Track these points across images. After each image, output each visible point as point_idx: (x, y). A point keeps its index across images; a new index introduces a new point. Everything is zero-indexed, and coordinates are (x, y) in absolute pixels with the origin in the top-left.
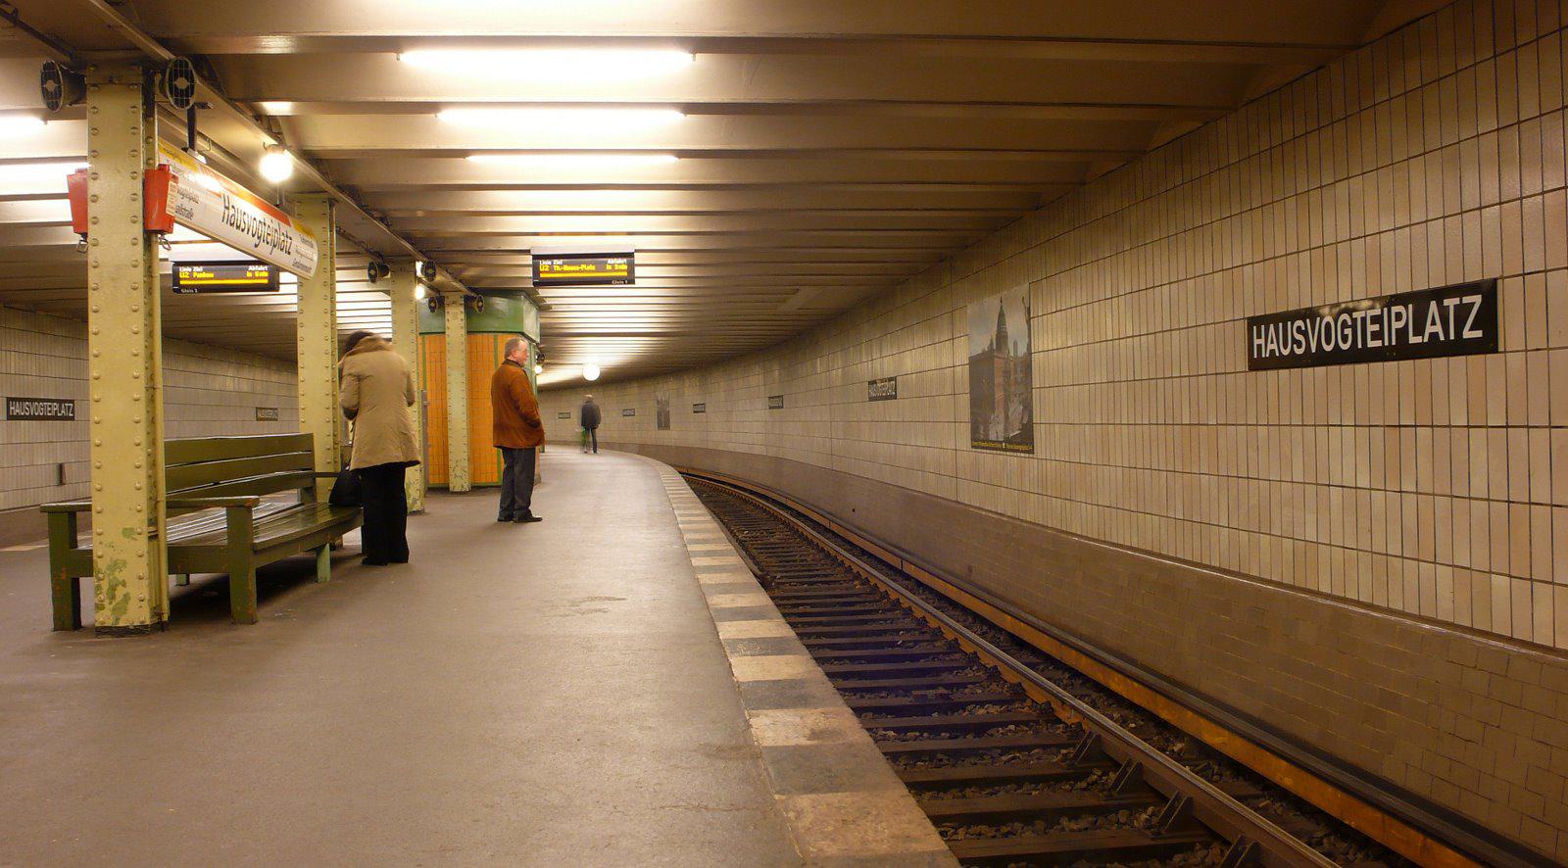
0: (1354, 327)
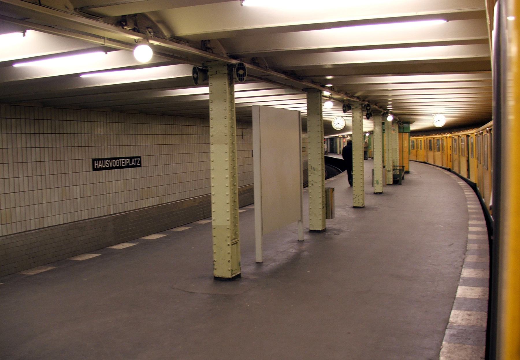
0: (119, 162)
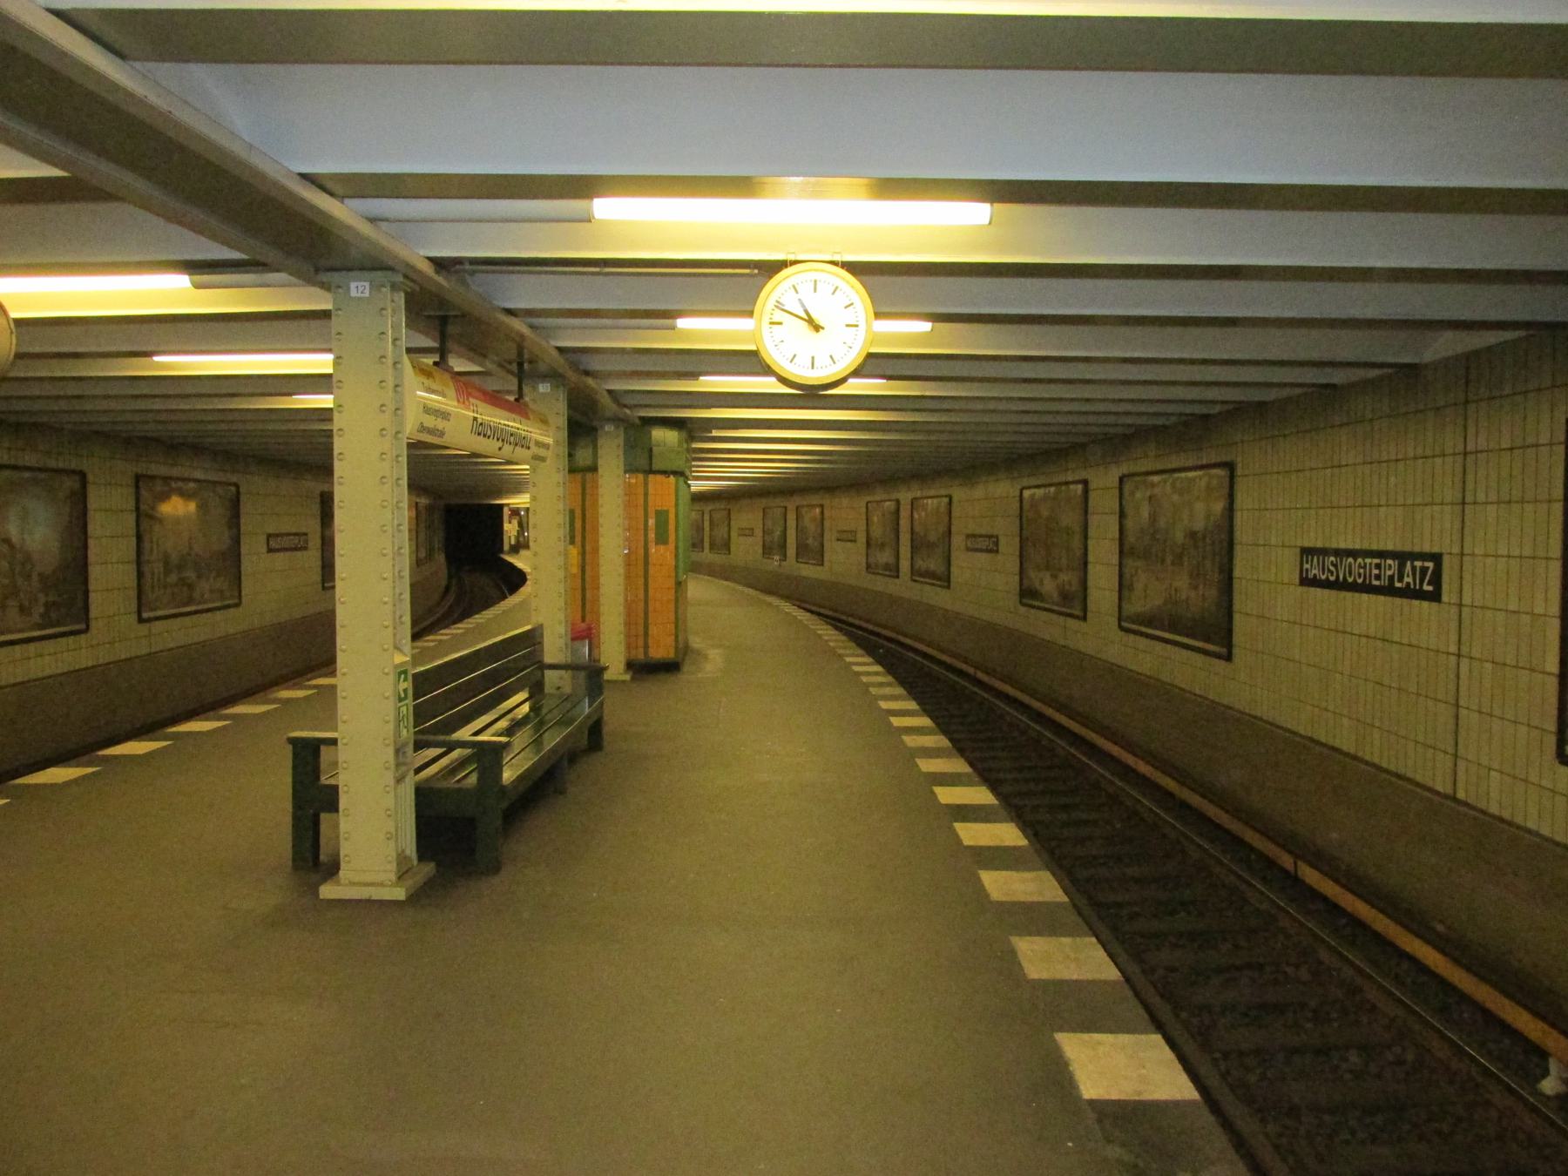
0: (1365, 567)
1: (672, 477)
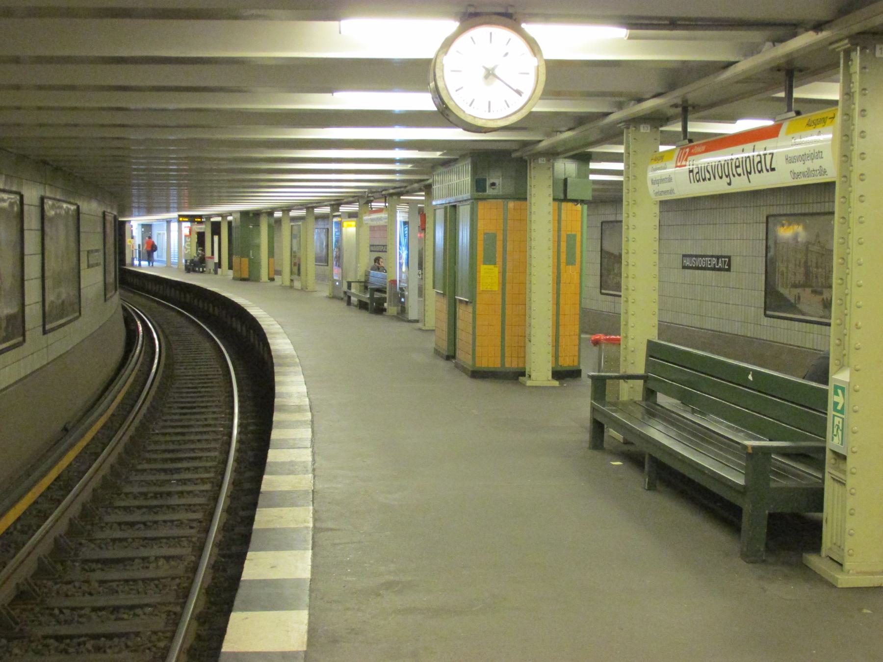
1: (579, 205)
